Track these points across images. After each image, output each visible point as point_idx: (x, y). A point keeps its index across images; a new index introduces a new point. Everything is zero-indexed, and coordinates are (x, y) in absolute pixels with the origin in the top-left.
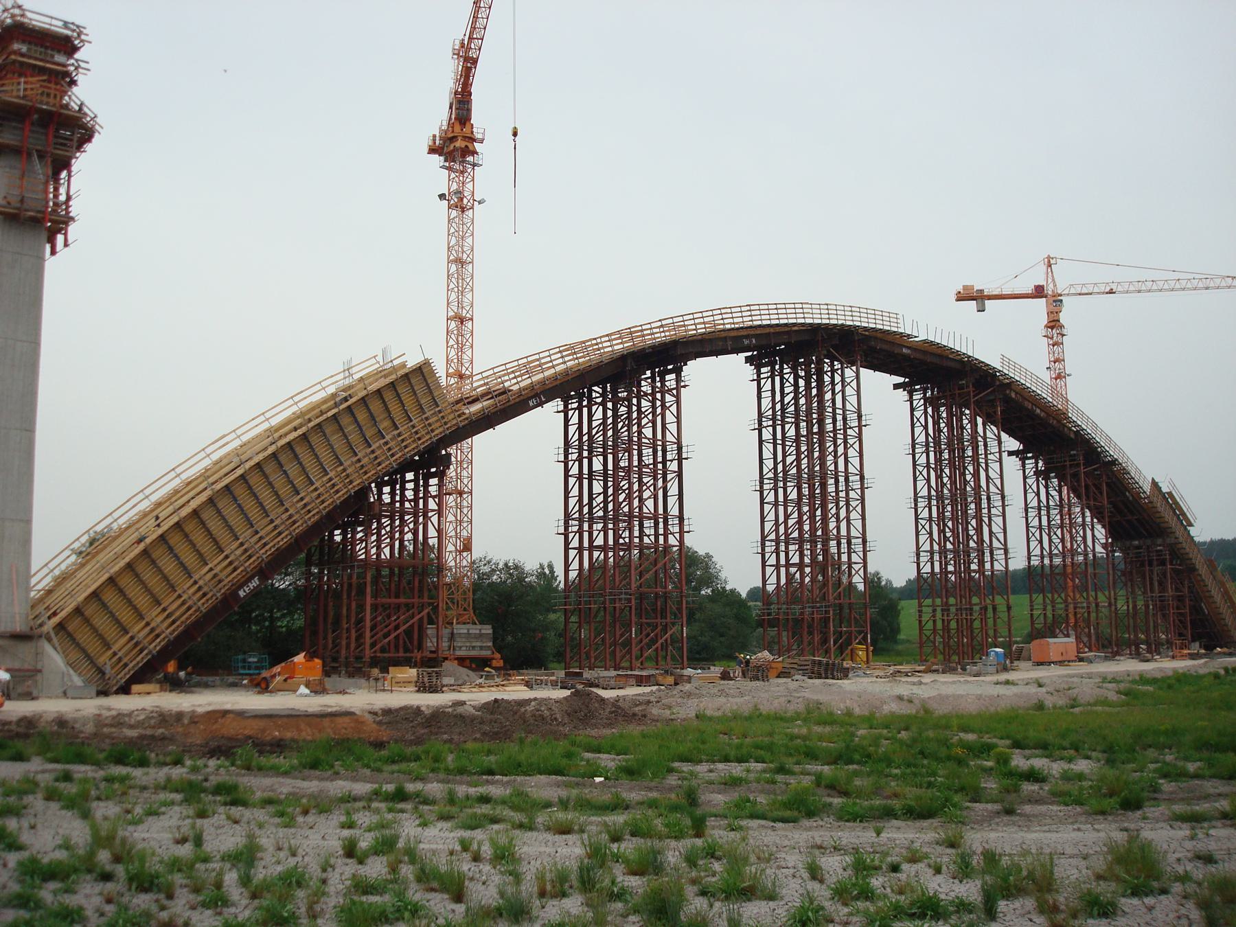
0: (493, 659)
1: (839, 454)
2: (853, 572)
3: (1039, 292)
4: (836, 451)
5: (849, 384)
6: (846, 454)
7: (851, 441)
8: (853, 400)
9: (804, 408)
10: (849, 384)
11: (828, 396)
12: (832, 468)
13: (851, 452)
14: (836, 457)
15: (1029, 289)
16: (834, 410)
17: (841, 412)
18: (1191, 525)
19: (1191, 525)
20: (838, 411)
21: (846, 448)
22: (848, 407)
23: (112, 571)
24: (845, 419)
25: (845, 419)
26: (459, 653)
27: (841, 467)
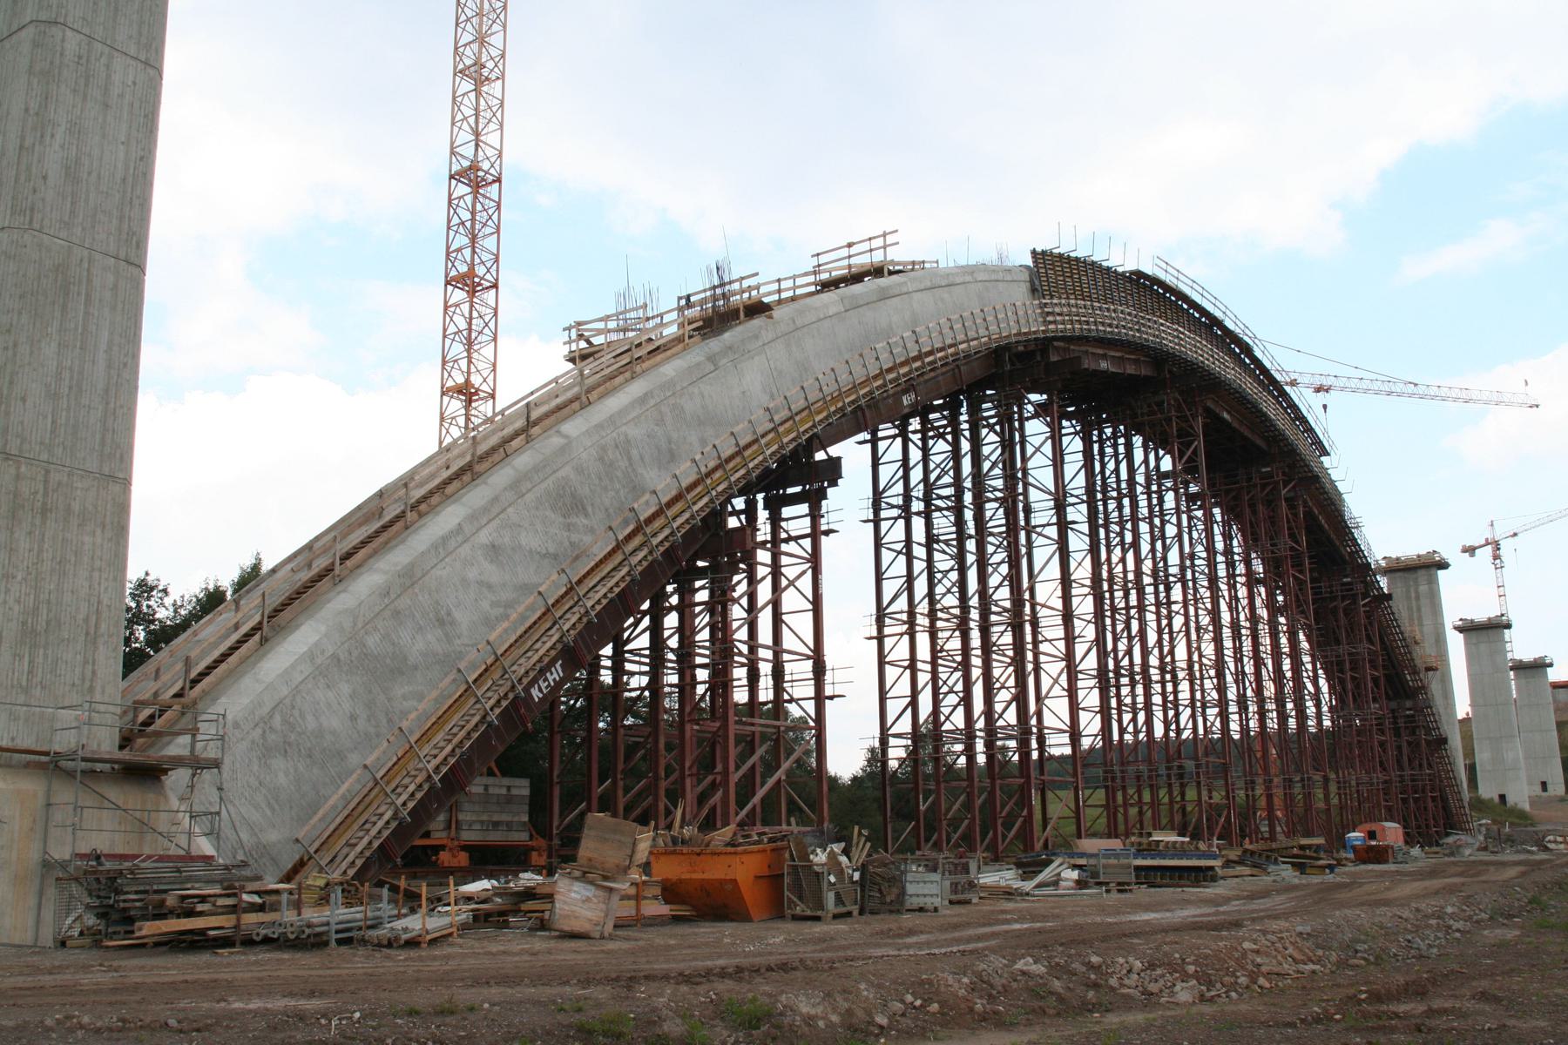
0: (533, 849)
1: (760, 603)
2: (784, 582)
3: (1487, 544)
4: (752, 596)
5: (791, 583)
6: (776, 604)
7: (789, 572)
8: (801, 624)
9: (673, 643)
10: (791, 583)
11: (737, 613)
12: (742, 634)
13: (790, 600)
14: (752, 608)
15: (1483, 542)
16: (753, 649)
17: (768, 654)
18: (1326, 453)
19: (1326, 453)
20: (763, 653)
21: (776, 588)
22: (789, 641)
23: (239, 976)
24: (778, 674)
25: (778, 674)
26: (468, 836)
27: (765, 634)
